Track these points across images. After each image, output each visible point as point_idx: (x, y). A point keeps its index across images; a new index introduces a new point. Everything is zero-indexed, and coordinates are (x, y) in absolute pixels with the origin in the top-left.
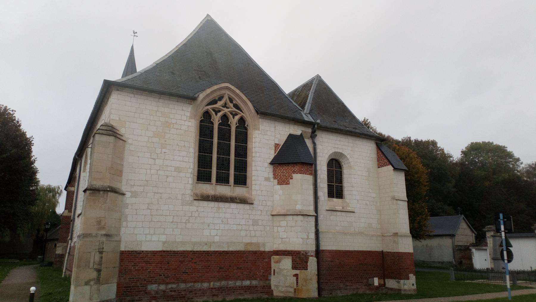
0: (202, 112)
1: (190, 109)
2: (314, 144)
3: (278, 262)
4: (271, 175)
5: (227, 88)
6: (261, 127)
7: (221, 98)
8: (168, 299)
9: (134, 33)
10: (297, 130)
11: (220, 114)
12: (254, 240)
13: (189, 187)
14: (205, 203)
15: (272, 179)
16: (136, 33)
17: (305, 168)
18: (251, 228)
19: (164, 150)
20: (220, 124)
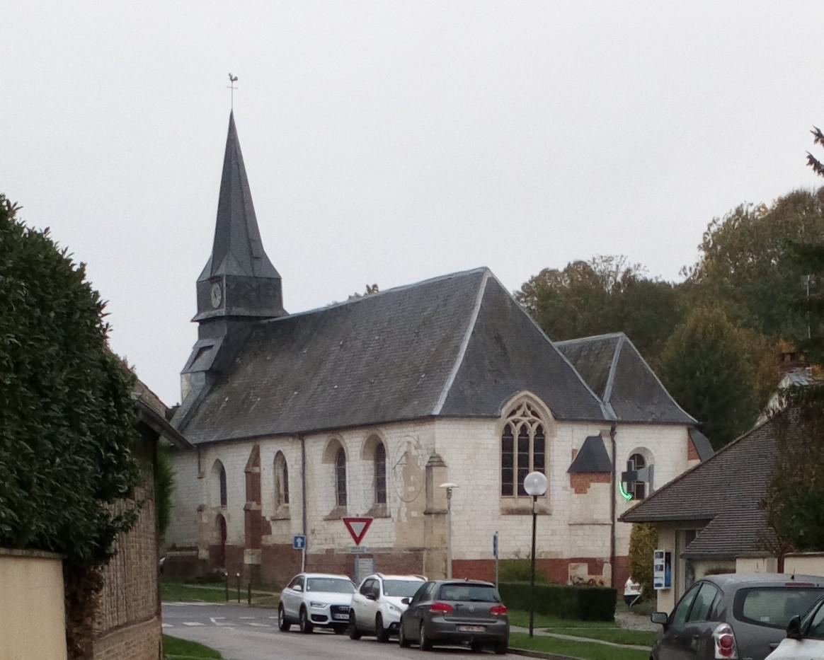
0: (504, 425)
1: (494, 427)
2: (614, 442)
3: (575, 568)
4: (569, 484)
5: (527, 396)
6: (559, 433)
7: (519, 408)
8: (107, 650)
9: (232, 80)
10: (594, 431)
11: (520, 425)
12: (553, 549)
13: (498, 502)
14: (511, 517)
15: (569, 488)
16: (236, 79)
17: (603, 476)
18: (550, 538)
19: (476, 471)
20: (520, 436)
